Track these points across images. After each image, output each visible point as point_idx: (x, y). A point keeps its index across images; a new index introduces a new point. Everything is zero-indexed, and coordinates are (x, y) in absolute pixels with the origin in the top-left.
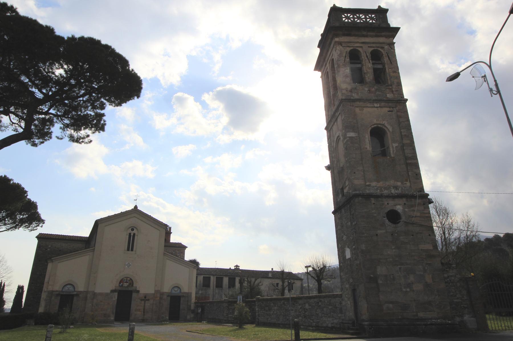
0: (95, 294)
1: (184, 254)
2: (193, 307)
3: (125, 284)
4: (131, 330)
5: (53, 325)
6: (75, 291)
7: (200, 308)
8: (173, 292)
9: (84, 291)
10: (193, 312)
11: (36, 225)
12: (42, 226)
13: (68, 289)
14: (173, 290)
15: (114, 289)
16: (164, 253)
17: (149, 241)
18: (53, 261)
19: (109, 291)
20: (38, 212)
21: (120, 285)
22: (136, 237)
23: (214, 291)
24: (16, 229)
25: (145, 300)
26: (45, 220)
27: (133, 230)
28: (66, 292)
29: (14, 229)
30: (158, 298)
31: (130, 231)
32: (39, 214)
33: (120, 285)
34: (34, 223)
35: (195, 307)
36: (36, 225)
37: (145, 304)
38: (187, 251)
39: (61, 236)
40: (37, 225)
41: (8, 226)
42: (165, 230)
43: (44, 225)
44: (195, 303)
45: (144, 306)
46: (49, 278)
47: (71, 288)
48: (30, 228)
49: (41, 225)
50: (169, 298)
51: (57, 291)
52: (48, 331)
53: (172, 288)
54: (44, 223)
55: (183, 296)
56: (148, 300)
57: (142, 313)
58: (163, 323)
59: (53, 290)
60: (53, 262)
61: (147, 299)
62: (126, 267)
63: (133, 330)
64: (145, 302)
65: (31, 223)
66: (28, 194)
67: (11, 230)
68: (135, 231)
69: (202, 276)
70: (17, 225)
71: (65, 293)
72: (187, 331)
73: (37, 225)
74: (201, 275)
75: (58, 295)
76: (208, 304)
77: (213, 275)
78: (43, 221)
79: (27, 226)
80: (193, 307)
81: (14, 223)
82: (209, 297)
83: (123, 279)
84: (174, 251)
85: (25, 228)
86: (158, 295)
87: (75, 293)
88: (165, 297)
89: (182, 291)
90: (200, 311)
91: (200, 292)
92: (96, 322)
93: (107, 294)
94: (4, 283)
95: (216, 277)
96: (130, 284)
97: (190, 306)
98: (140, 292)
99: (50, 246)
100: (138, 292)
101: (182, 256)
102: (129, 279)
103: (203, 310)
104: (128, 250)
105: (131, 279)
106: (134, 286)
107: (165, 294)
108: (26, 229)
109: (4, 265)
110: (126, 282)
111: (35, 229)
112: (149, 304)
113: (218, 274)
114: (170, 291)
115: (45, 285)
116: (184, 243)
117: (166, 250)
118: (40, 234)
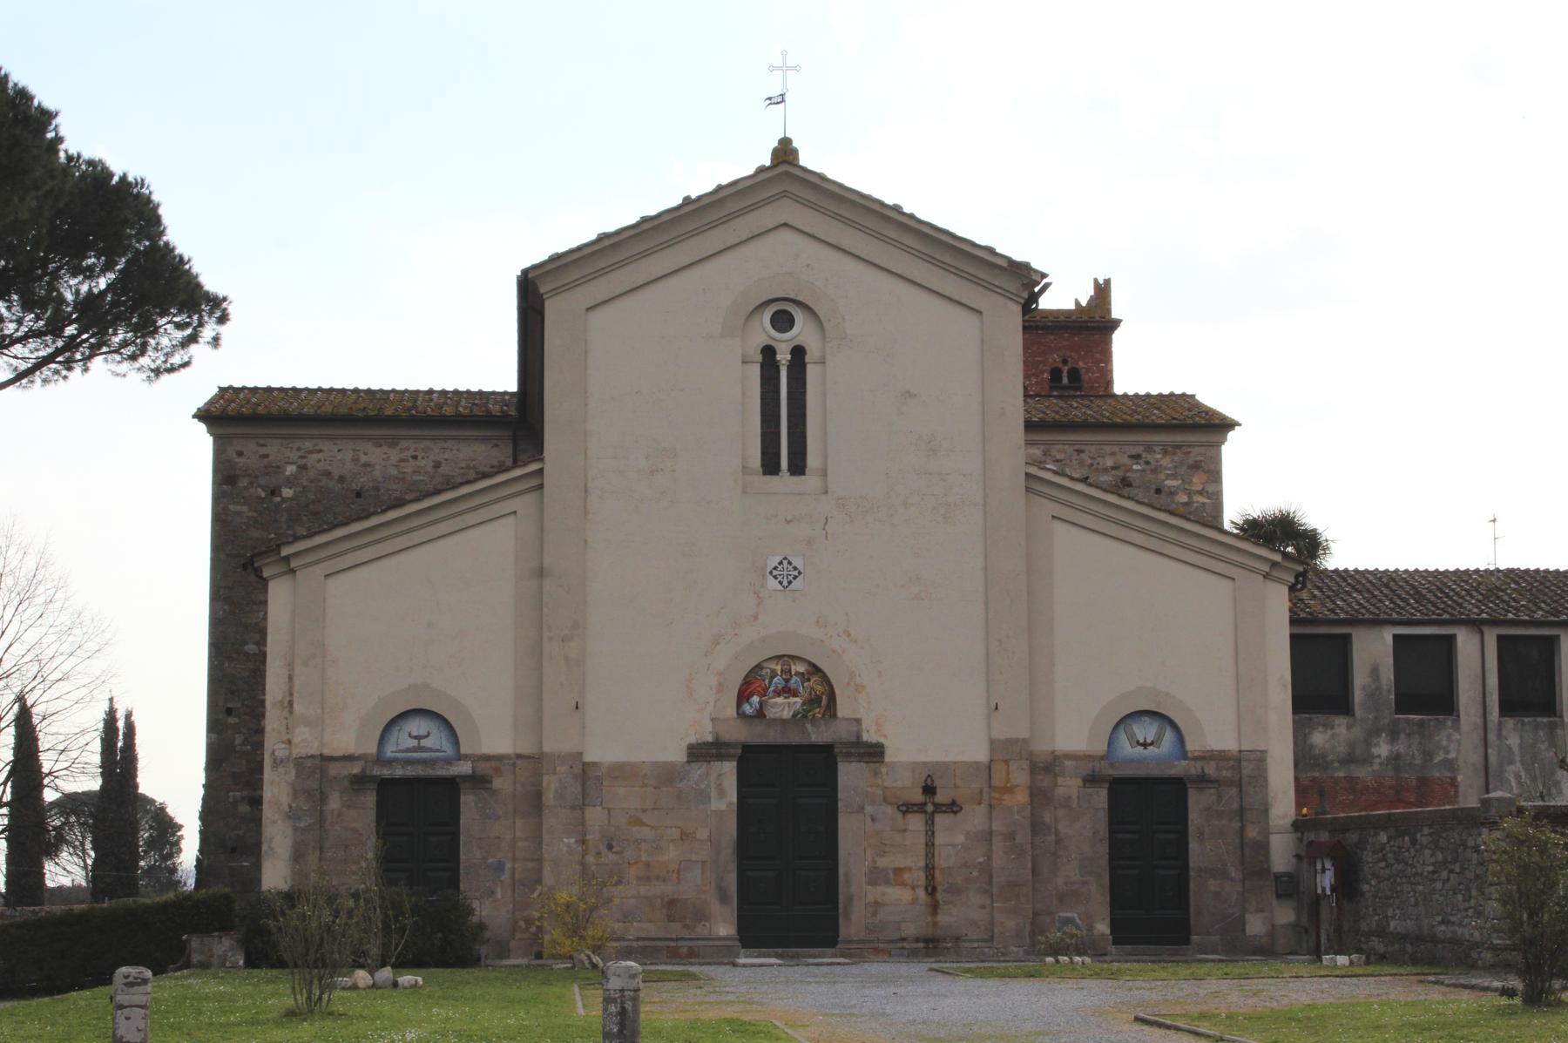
0: (586, 775)
1: (1215, 476)
2: (1281, 853)
3: (780, 700)
4: (613, 1009)
5: (142, 969)
6: (459, 757)
7: (1328, 865)
8: (1126, 749)
9: (519, 756)
10: (1288, 887)
11: (179, 335)
12: (216, 341)
13: (414, 743)
14: (1123, 738)
15: (710, 739)
16: (1028, 475)
17: (909, 395)
18: (293, 564)
19: (675, 754)
20: (169, 249)
21: (747, 709)
22: (812, 372)
23: (1492, 737)
24: (70, 369)
25: (930, 808)
26: (225, 299)
27: (783, 321)
28: (409, 762)
29: (57, 372)
30: (1022, 797)
31: (763, 331)
32: (181, 258)
33: (747, 709)
34: (164, 320)
35: (1298, 857)
36: (179, 335)
37: (930, 833)
38: (1233, 452)
39: (354, 397)
40: (189, 331)
41: (17, 349)
42: (1017, 309)
43: (224, 330)
44: (1299, 826)
45: (930, 846)
46: (290, 678)
47: (436, 740)
48: (144, 361)
49: (208, 333)
50: (1101, 796)
51: (350, 758)
52: (121, 1007)
53: (1116, 728)
54: (223, 319)
55: (1203, 780)
56: (953, 807)
57: (921, 893)
58: (1050, 959)
59: (327, 752)
60: (293, 571)
61: (939, 798)
62: (772, 584)
63: (629, 1005)
64: (930, 823)
65: (146, 329)
66: (62, 133)
67: (45, 381)
68: (802, 331)
69: (1388, 635)
70: (72, 344)
71: (399, 772)
72: (1137, 1019)
73: (189, 331)
74: (1376, 622)
75: (359, 781)
76: (1383, 837)
77: (1476, 625)
78: (216, 307)
79: (125, 344)
80: (1281, 853)
81: (54, 329)
82: (1453, 783)
83: (758, 667)
84: (1136, 457)
85: (118, 357)
86: (1020, 777)
87: (465, 768)
88: (1069, 786)
89: (1191, 746)
90: (1326, 880)
91: (1383, 749)
92: (597, 949)
93: (667, 775)
94: (129, 716)
95: (1500, 638)
96: (813, 701)
97: (1263, 847)
98: (889, 757)
99: (290, 470)
100: (874, 753)
101: (1200, 493)
102: (801, 668)
103: (1347, 884)
104: (770, 466)
105: (816, 670)
106: (840, 714)
107: (1068, 763)
108: (126, 366)
109: (58, 605)
110: (787, 691)
111: (176, 359)
112: (961, 839)
113: (1510, 616)
114: (1101, 747)
115: (273, 721)
116: (1212, 398)
117: (1080, 452)
118: (223, 391)
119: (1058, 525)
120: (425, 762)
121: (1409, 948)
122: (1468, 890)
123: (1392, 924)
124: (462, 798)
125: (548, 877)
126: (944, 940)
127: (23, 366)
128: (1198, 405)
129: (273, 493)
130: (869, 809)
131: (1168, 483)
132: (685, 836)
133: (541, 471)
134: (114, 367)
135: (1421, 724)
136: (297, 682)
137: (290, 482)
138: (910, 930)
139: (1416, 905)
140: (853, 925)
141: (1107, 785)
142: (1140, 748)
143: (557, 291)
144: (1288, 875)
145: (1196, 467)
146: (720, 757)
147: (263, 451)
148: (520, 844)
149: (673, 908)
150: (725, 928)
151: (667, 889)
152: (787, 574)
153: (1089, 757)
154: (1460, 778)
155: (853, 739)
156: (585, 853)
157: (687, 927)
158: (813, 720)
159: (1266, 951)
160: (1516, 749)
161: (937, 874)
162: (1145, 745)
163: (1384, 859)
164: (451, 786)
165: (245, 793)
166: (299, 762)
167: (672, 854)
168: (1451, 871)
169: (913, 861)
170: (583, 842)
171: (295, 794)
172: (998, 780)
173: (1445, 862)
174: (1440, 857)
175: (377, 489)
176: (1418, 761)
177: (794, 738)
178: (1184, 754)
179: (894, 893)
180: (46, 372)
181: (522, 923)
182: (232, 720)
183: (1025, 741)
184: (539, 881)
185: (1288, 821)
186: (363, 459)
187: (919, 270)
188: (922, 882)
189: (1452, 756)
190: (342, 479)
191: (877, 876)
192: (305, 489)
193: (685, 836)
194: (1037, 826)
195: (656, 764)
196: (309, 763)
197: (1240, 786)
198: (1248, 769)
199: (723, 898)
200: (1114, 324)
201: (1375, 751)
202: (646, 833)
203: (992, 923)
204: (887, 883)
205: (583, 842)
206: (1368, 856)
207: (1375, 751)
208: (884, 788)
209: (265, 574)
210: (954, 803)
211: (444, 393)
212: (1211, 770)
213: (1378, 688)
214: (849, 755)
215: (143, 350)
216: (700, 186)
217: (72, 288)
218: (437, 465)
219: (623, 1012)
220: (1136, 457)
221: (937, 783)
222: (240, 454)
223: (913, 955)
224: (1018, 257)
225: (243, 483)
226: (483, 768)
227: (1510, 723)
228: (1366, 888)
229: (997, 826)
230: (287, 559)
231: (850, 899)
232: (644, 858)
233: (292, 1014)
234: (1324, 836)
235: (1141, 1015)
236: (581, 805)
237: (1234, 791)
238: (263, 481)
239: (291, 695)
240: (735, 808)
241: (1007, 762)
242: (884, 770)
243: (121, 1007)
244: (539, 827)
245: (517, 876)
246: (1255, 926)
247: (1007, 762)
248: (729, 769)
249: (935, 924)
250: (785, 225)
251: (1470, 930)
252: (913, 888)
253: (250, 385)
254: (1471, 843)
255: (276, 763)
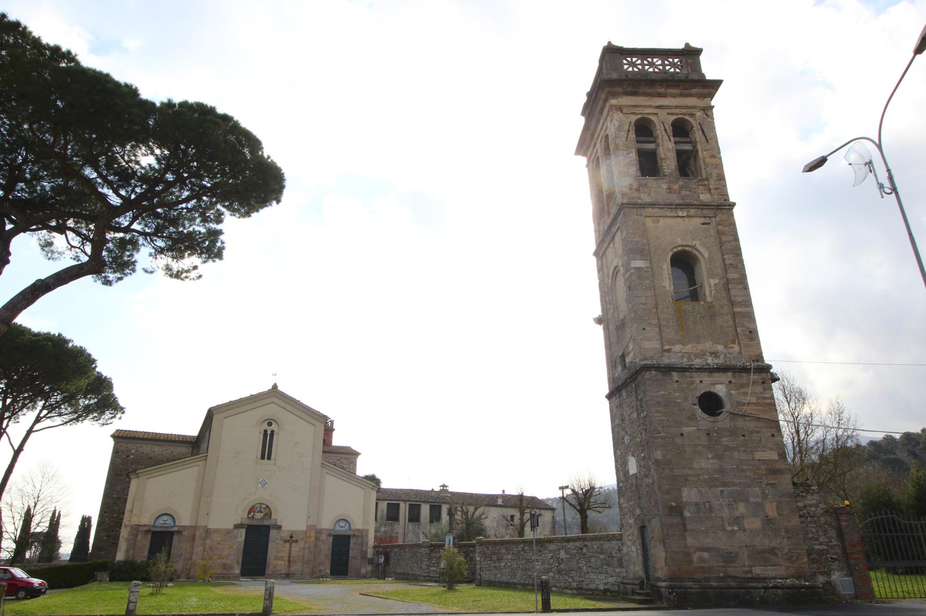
0: (207, 531)
1: (355, 465)
4: (268, 592)
5: (138, 582)
6: (175, 526)
7: (383, 556)
8: (338, 528)
9: (191, 526)
10: (371, 562)
13: (163, 522)
15: (240, 523)
16: (322, 463)
17: (297, 443)
18: (139, 475)
21: (250, 516)
22: (275, 436)
23: (406, 527)
25: (291, 541)
27: (270, 424)
30: (313, 539)
31: (265, 426)
35: (374, 554)
36: (111, 416)
37: (290, 547)
38: (360, 461)
40: (113, 415)
41: (65, 416)
42: (324, 426)
43: (123, 415)
44: (374, 547)
45: (290, 551)
46: (133, 504)
47: (169, 522)
48: (100, 421)
49: (118, 416)
50: (331, 539)
51: (145, 526)
52: (132, 592)
55: (354, 535)
56: (296, 541)
57: (287, 563)
58: (321, 579)
59: (140, 524)
60: (138, 477)
61: (293, 539)
62: (260, 486)
63: (272, 591)
64: (291, 545)
65: (102, 413)
67: (71, 425)
68: (274, 427)
69: (386, 503)
71: (158, 529)
72: (360, 594)
73: (113, 415)
75: (147, 532)
76: (396, 550)
77: (405, 501)
78: (122, 410)
79: (95, 417)
81: (75, 412)
82: (397, 537)
83: (254, 506)
84: (338, 460)
85: (92, 420)
86: (313, 534)
87: (176, 529)
88: (324, 537)
90: (382, 560)
91: (383, 529)
93: (228, 532)
94: (60, 512)
95: (409, 504)
96: (266, 514)
97: (366, 552)
99: (133, 451)
100: (279, 528)
102: (264, 506)
104: (263, 458)
105: (268, 507)
106: (272, 517)
107: (324, 531)
110: (260, 512)
111: (109, 422)
116: (355, 448)
118: (117, 431)
119: (328, 475)
120: (166, 527)
121: (402, 576)
122: (418, 562)
123: (397, 570)
124: (174, 537)
125: (194, 557)
126: (291, 574)
127: (65, 420)
128: (352, 449)
129: (128, 456)
130: (277, 541)
131: (345, 466)
132: (231, 547)
133: (207, 456)
134: (91, 422)
135: (391, 523)
136: (135, 505)
137: (133, 454)
138: (283, 572)
139: (404, 566)
140: (269, 570)
141: (151, 533)
142: (341, 528)
143: (218, 413)
144: (371, 559)
145: (351, 463)
146: (242, 528)
147: (127, 446)
148: (187, 549)
149: (225, 566)
150: (237, 571)
151: (224, 561)
152: (264, 484)
153: (328, 530)
154: (399, 536)
155: (275, 524)
156: (204, 551)
157: (228, 571)
158: (266, 519)
159: (364, 577)
160: (411, 530)
161: (291, 558)
162: (342, 527)
163: (397, 555)
164: (172, 534)
165: (106, 534)
166: (132, 526)
167: (226, 552)
168: (414, 558)
169: (286, 554)
170: (204, 549)
171: (129, 535)
172: (308, 535)
173: (412, 556)
174: (411, 555)
175: (156, 457)
176: (390, 532)
177: (260, 523)
178: (350, 530)
179: (280, 562)
180: (71, 422)
181: (185, 570)
182: (106, 514)
183: (315, 525)
184: (191, 559)
185: (372, 546)
186: (153, 449)
187: (304, 416)
188: (287, 560)
189: (397, 531)
190: (146, 454)
191: (277, 558)
192: (137, 456)
193: (231, 547)
194: (316, 546)
195: (225, 529)
196: (135, 526)
197: (362, 537)
198: (364, 533)
199: (238, 564)
200: (334, 430)
201: (381, 529)
202: (220, 546)
203: (303, 570)
204: (279, 560)
205: (204, 549)
206: (392, 554)
207: (381, 529)
208: (281, 536)
209: (131, 477)
210: (297, 540)
211: (175, 435)
212: (356, 533)
213: (383, 515)
214: (273, 528)
215: (100, 420)
216: (255, 392)
217: (83, 402)
218: (172, 452)
219: (270, 593)
220: (338, 460)
221: (293, 536)
222: (121, 446)
223: (283, 578)
224: (325, 414)
225: (120, 454)
226: (181, 529)
227: (410, 523)
228: (391, 562)
229: (306, 546)
230: (138, 474)
231: (269, 564)
232: (219, 553)
233: (152, 594)
234: (381, 550)
235: (362, 593)
236: (206, 538)
237: (361, 539)
238: (125, 453)
239: (133, 508)
240: (244, 541)
241: (310, 530)
242: (281, 532)
243: (132, 592)
244: (193, 544)
245: (186, 557)
246: (363, 571)
247: (310, 530)
248: (243, 531)
249: (289, 570)
250: (273, 402)
251: (418, 572)
252: (285, 561)
253: (125, 429)
254: (419, 551)
255: (126, 526)
